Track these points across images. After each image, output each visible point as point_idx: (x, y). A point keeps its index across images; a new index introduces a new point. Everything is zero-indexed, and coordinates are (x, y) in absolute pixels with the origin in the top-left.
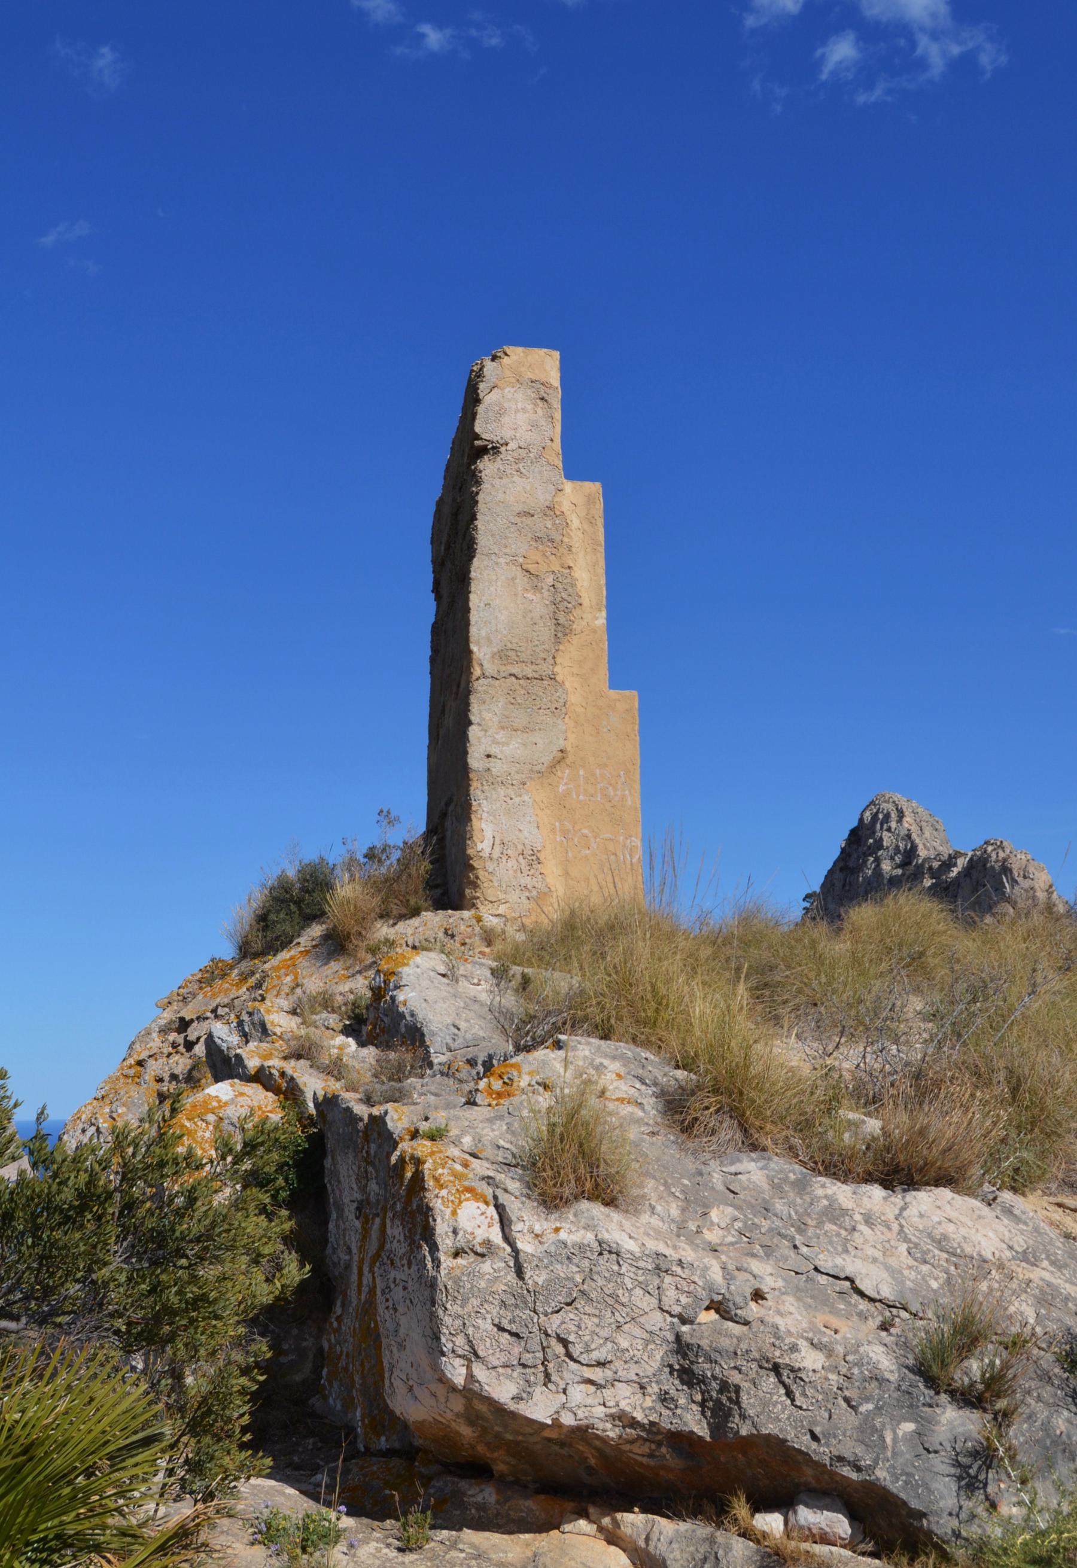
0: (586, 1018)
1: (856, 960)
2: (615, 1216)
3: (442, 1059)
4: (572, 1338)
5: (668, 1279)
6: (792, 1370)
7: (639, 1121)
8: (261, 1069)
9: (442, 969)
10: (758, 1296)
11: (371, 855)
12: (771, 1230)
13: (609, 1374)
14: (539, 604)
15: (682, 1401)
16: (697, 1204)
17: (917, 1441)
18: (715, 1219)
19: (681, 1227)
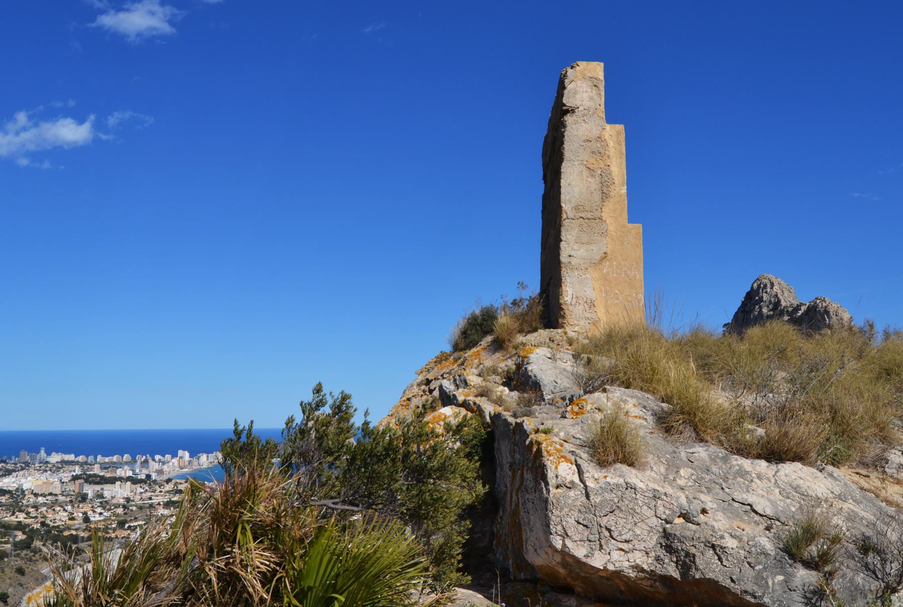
0: (618, 379)
1: (751, 353)
2: (634, 471)
3: (549, 397)
4: (613, 528)
5: (659, 502)
6: (721, 547)
7: (645, 427)
8: (465, 401)
9: (549, 355)
10: (704, 511)
11: (514, 303)
12: (710, 480)
13: (631, 546)
14: (594, 183)
15: (667, 561)
16: (673, 466)
17: (784, 585)
18: (682, 474)
19: (666, 478)
